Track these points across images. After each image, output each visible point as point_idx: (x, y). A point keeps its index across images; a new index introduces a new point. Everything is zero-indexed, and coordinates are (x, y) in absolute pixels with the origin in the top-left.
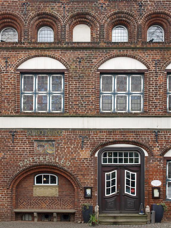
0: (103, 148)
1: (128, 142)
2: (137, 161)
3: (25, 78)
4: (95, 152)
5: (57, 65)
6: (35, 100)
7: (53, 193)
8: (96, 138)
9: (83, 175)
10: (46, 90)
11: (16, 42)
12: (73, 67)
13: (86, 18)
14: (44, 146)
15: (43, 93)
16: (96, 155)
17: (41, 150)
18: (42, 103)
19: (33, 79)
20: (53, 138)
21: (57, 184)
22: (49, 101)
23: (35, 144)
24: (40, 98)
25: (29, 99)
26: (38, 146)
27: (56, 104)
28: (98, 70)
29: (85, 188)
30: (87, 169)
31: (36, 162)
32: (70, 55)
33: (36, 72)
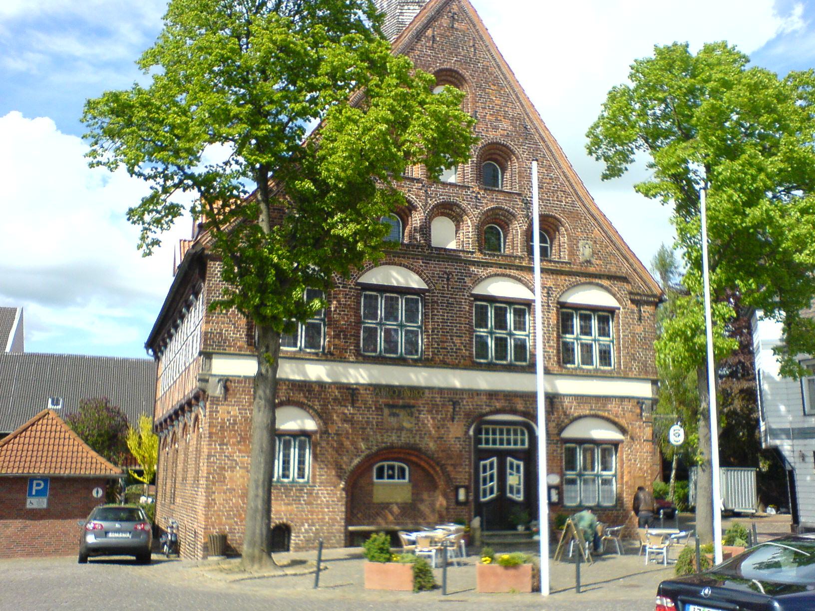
0: (479, 422)
1: (514, 412)
2: (523, 443)
3: (366, 296)
4: (469, 429)
5: (415, 282)
6: (381, 336)
7: (257, 507)
8: (467, 405)
9: (454, 466)
10: (396, 319)
11: (784, 330)
12: (439, 286)
13: (452, 210)
14: (398, 415)
15: (391, 325)
16: (471, 433)
17: (393, 420)
18: (391, 342)
19: (377, 299)
20: (412, 402)
21: (407, 480)
22: (401, 339)
23: (386, 411)
24: (387, 332)
25: (371, 334)
26: (390, 415)
27: (412, 344)
28: (472, 295)
29: (457, 489)
30: (460, 456)
31: (386, 443)
32: (436, 268)
33: (382, 289)
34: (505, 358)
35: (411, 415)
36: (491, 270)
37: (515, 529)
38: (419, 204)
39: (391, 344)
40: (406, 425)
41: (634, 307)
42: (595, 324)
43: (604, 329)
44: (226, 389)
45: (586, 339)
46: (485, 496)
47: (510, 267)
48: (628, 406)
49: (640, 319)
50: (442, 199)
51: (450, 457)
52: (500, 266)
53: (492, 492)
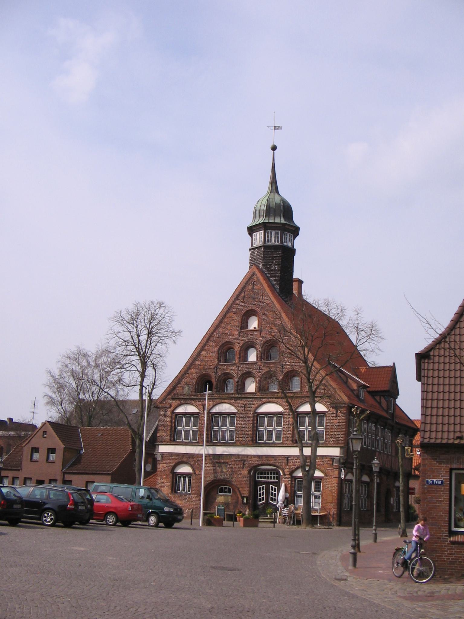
5: (233, 409)
6: (220, 433)
34: (271, 440)
35: (226, 466)
36: (264, 400)
37: (147, 520)
38: (235, 375)
39: (224, 438)
40: (224, 470)
41: (334, 410)
42: (228, 420)
43: (321, 423)
44: (162, 457)
45: (187, 428)
46: (260, 501)
47: (273, 398)
48: (326, 460)
49: (337, 416)
50: (245, 371)
51: (241, 484)
52: (268, 398)
53: (263, 500)
